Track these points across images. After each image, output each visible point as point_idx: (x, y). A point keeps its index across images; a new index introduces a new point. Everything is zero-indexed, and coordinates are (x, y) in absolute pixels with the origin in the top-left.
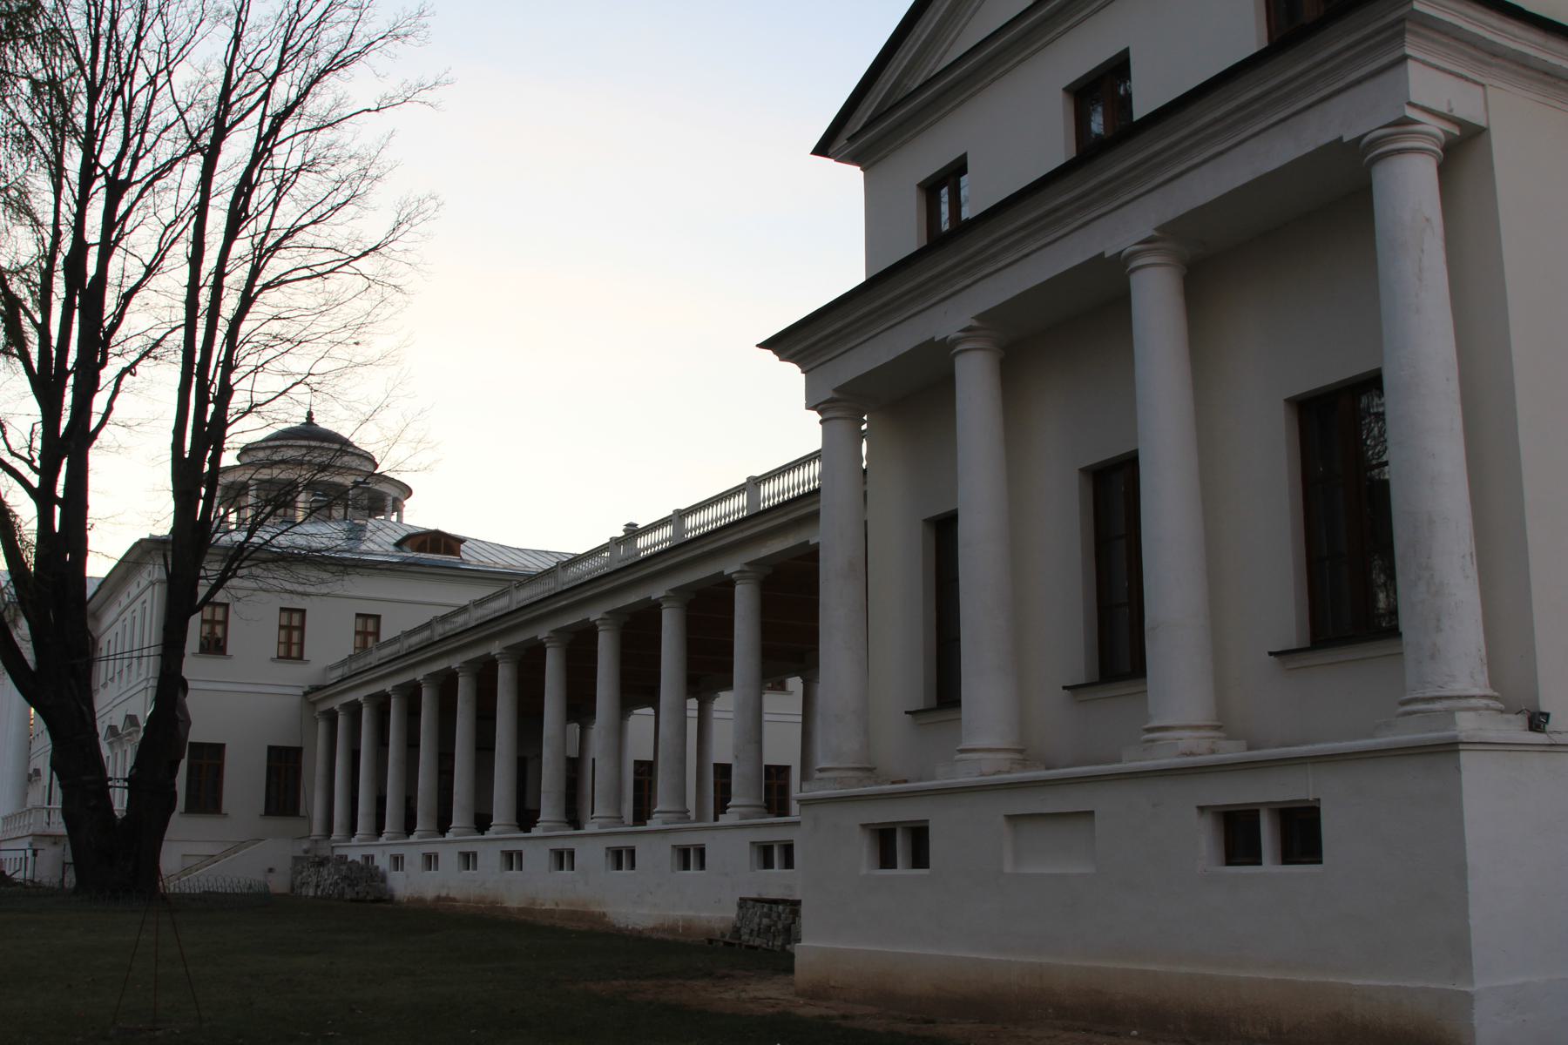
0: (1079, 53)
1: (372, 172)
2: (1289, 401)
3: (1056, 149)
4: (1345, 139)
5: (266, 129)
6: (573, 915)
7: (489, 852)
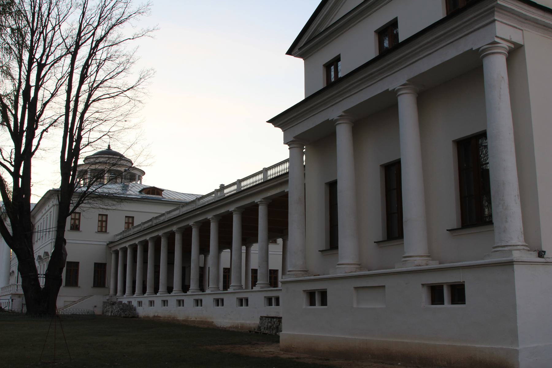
0: (380, 19)
1: (131, 61)
2: (454, 141)
3: (372, 52)
4: (474, 49)
5: (93, 45)
7: (172, 300)
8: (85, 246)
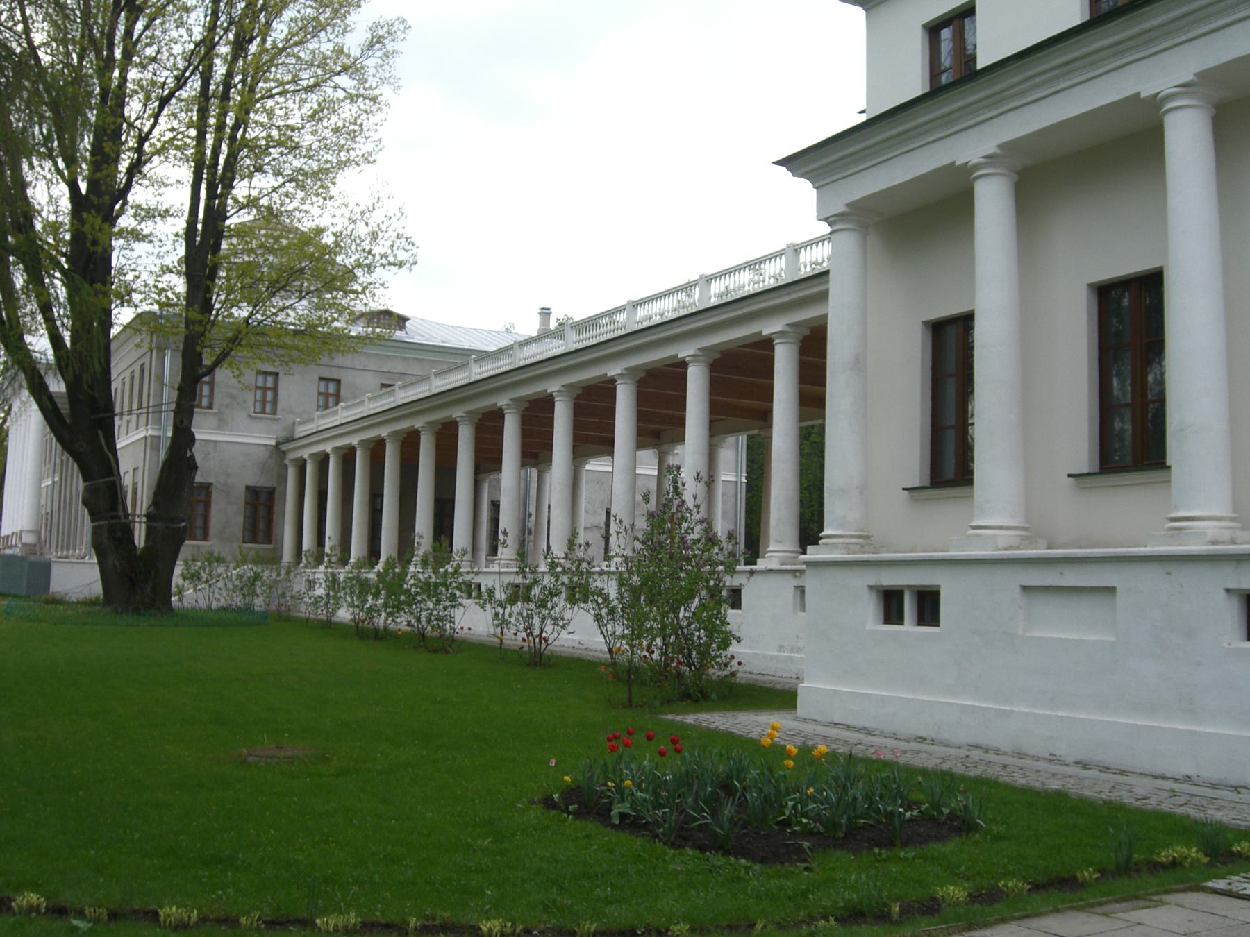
2: (1090, 286)
4: (1143, 95)
6: (728, 710)
8: (232, 440)
